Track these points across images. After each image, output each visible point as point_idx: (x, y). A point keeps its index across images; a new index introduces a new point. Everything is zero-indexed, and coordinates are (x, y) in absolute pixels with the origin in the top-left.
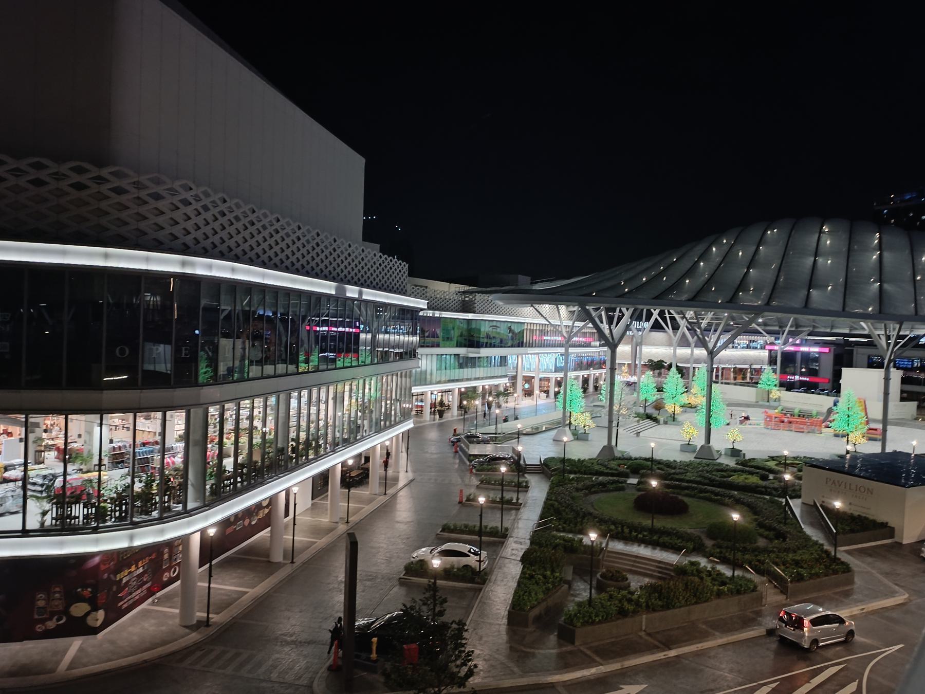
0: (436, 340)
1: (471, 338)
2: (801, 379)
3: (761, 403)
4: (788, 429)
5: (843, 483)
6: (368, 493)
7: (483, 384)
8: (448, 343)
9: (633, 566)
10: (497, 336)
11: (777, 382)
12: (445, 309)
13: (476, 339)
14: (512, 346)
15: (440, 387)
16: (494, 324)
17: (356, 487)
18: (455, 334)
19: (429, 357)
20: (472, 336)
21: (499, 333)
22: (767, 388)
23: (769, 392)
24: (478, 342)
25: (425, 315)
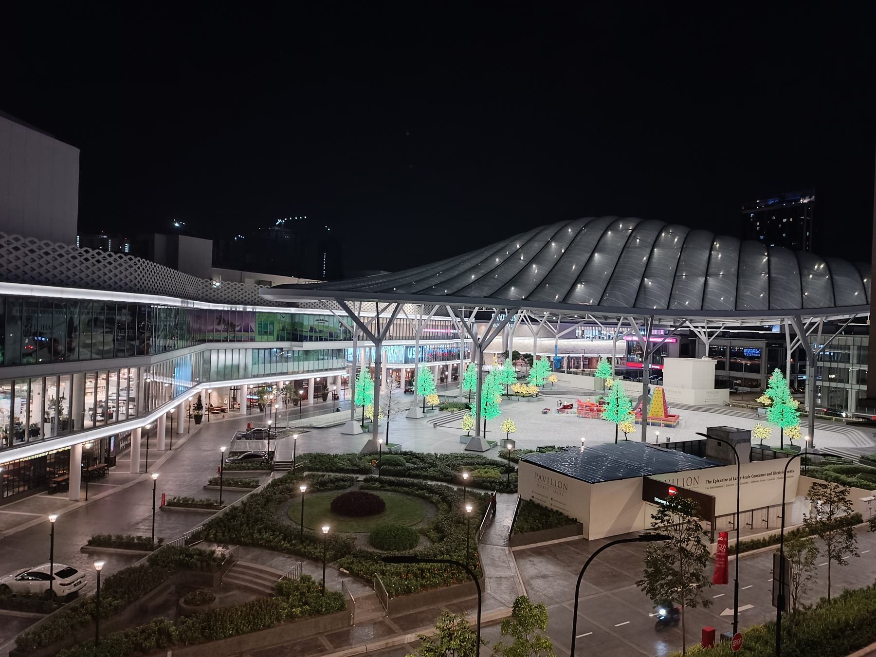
0: (250, 334)
1: (294, 332)
2: (653, 367)
3: (597, 391)
4: (597, 417)
5: (547, 478)
6: (68, 499)
7: (315, 377)
8: (265, 337)
9: (251, 582)
10: (325, 330)
11: (613, 371)
12: (265, 303)
13: (299, 333)
14: (345, 339)
15: (256, 381)
16: (322, 318)
17: (62, 492)
18: (277, 327)
19: (243, 352)
20: (296, 330)
21: (327, 327)
22: (603, 377)
23: (605, 381)
24: (301, 336)
25: (234, 309)
